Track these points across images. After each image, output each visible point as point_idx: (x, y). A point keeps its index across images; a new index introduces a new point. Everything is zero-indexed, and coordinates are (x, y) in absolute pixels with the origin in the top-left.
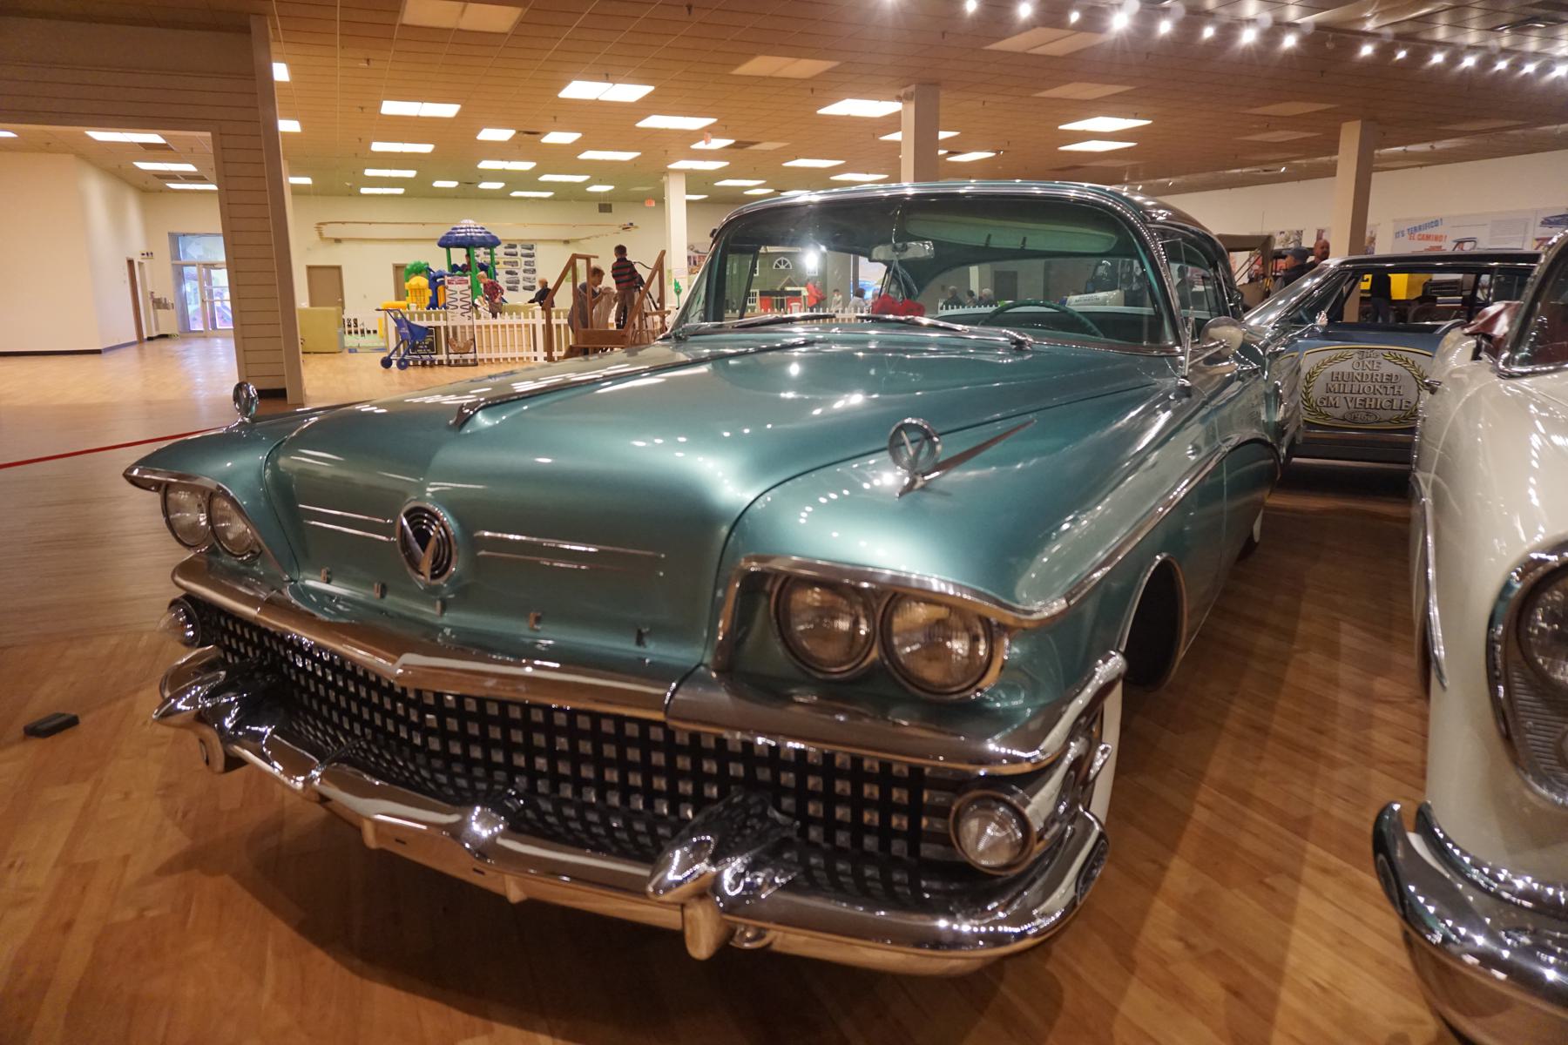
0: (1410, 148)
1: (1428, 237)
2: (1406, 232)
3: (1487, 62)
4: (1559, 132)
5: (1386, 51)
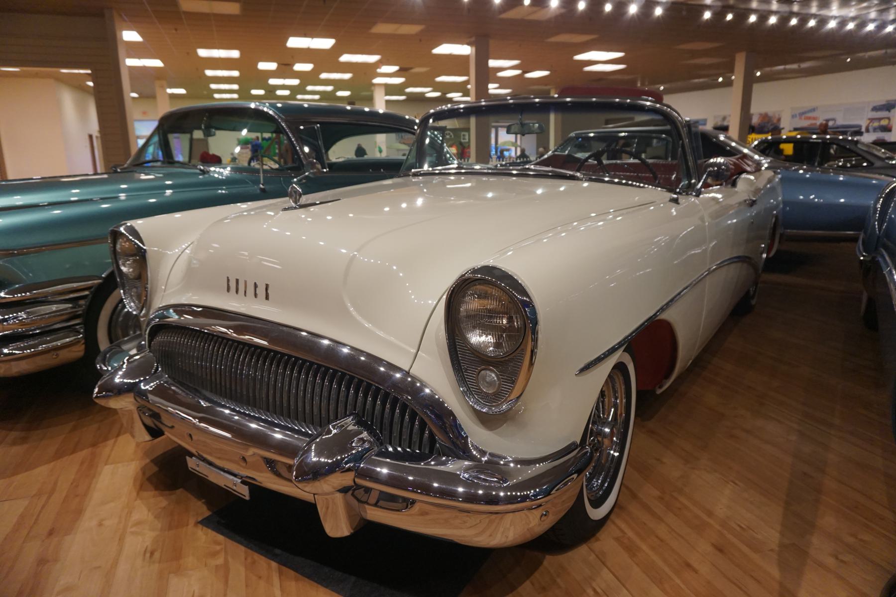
0: (788, 67)
1: (809, 118)
2: (798, 116)
3: (784, 19)
4: (867, 57)
5: (719, 14)
